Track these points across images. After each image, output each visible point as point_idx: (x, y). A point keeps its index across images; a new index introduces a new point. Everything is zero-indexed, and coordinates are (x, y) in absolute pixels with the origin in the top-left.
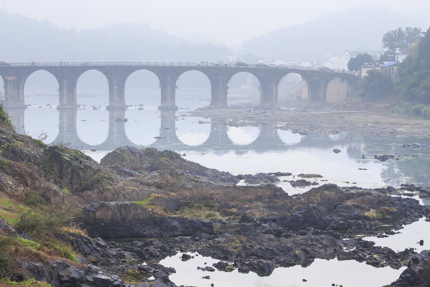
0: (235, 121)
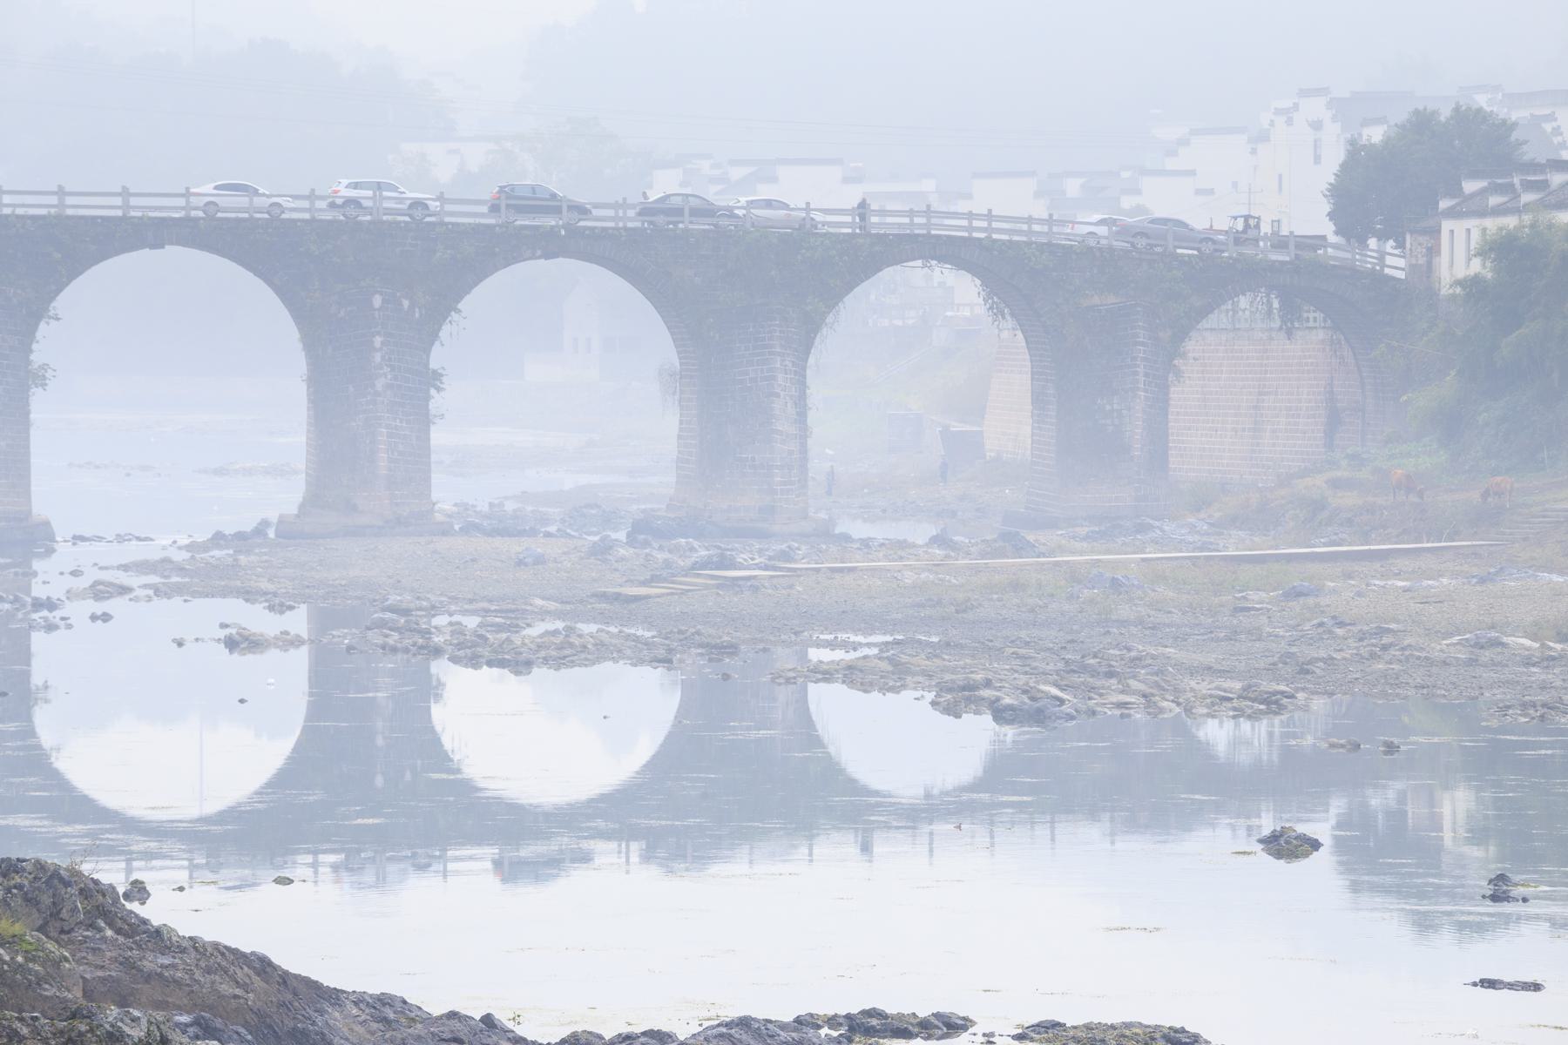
0: (500, 628)
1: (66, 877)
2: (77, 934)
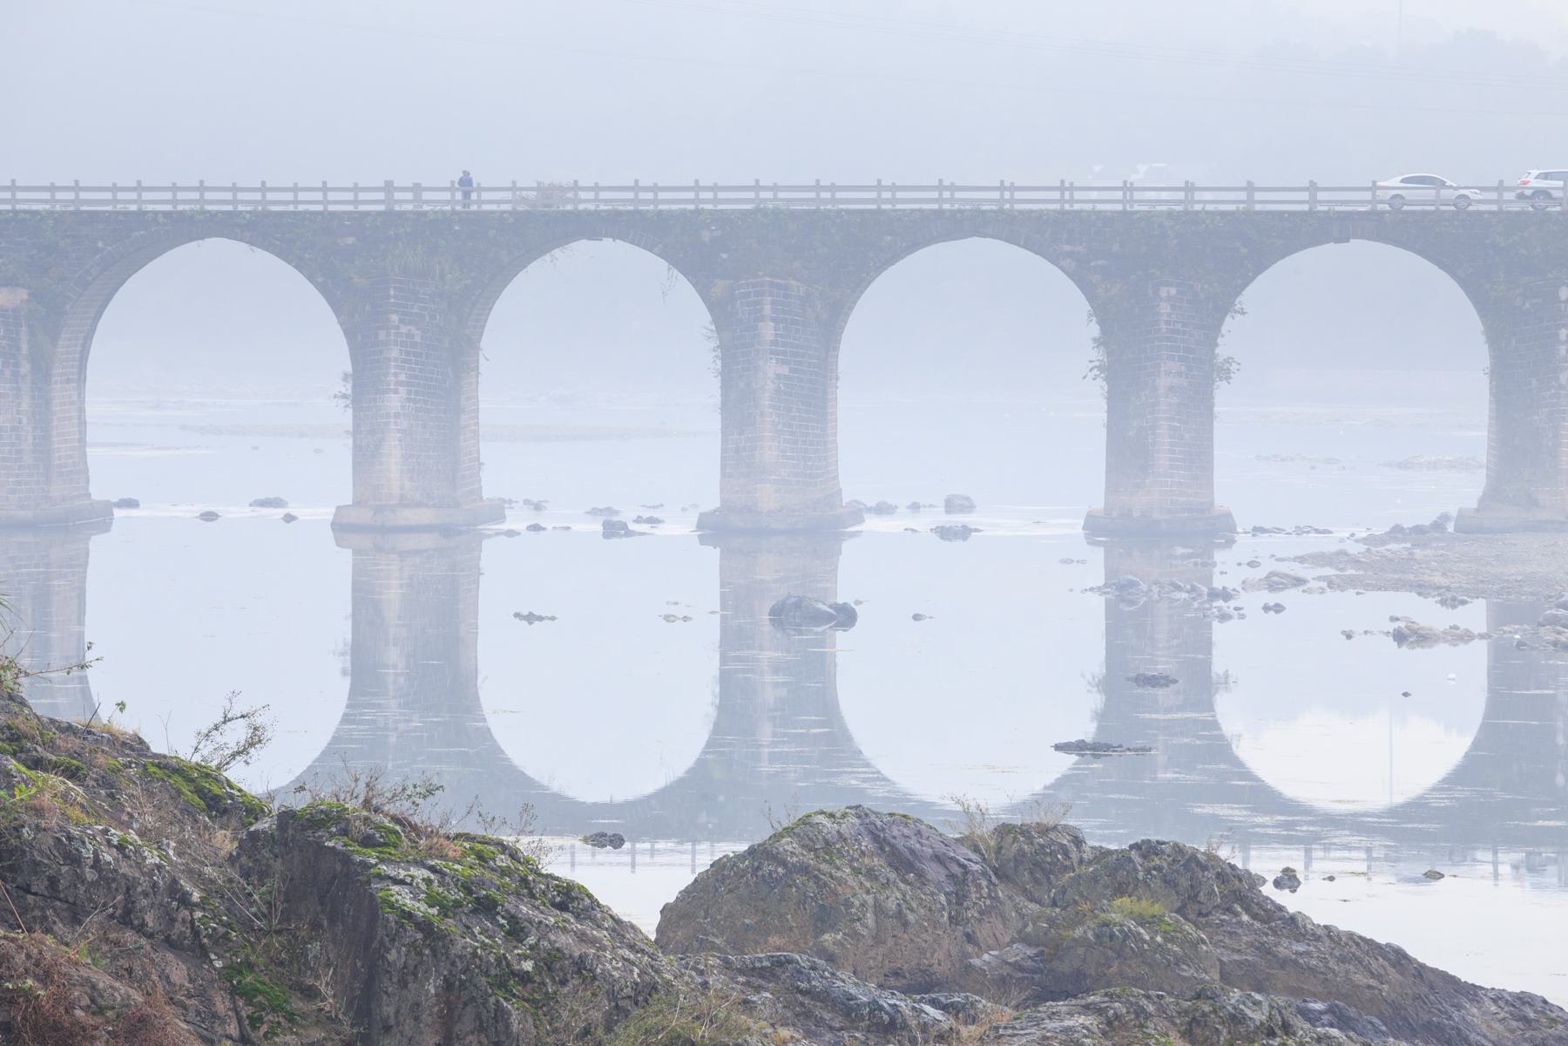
1: (1203, 861)
2: (1214, 918)
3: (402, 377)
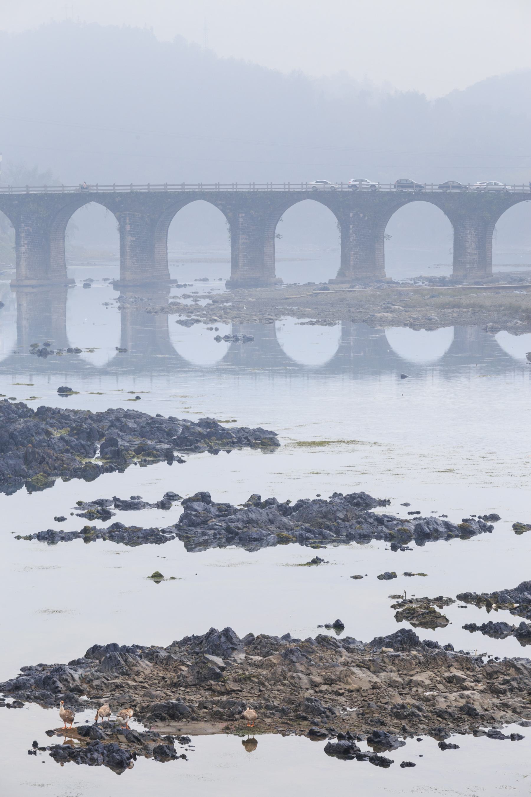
3: (26, 242)
